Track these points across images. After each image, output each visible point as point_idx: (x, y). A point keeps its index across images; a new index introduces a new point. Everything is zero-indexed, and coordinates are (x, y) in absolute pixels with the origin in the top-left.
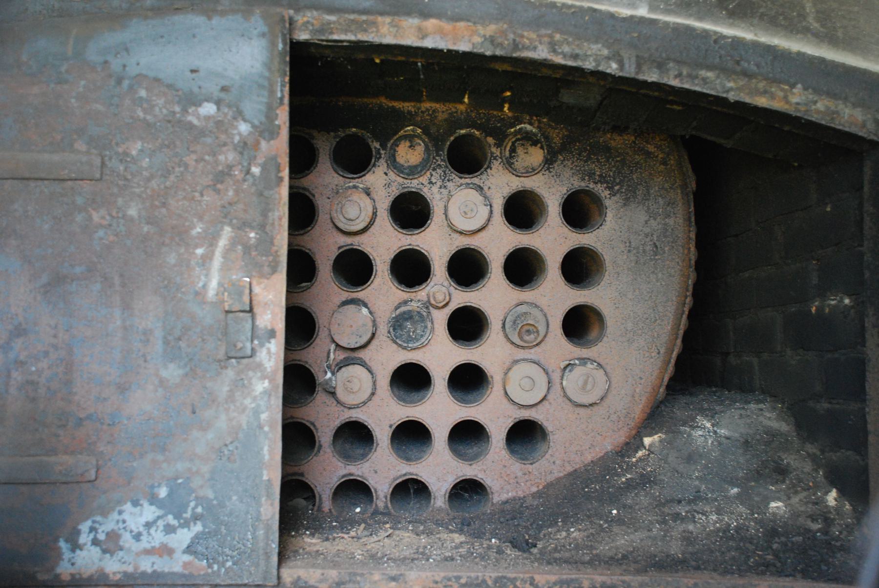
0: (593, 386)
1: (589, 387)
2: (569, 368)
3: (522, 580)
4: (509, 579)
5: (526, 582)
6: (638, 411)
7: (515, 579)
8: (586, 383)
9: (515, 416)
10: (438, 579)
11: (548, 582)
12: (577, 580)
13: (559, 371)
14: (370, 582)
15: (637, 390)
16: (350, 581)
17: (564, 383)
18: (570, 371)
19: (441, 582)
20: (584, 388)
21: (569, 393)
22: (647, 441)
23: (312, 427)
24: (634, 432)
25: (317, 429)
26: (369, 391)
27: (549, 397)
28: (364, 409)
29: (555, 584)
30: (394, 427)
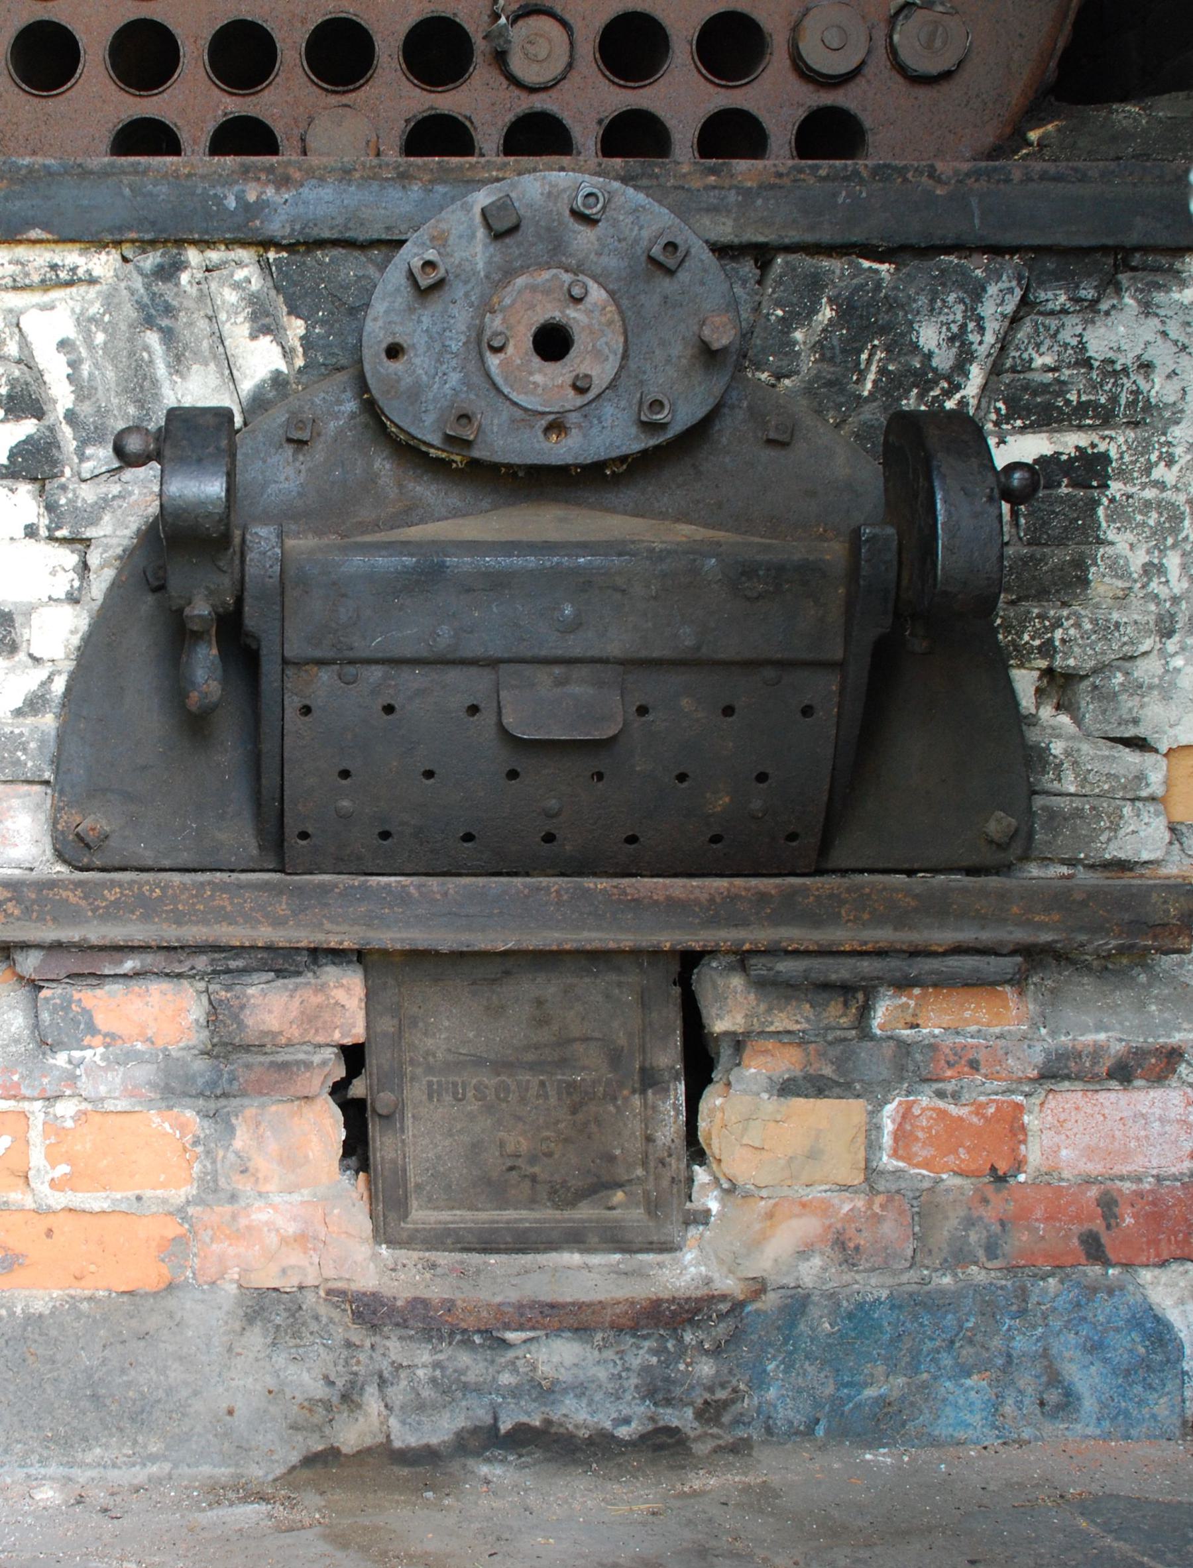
0: (945, 43)
1: (938, 43)
2: (905, 12)
3: (916, 170)
4: (895, 169)
5: (922, 174)
6: (1016, 94)
7: (905, 167)
8: (932, 37)
9: (809, 104)
10: (782, 170)
11: (956, 172)
12: (1003, 168)
13: (882, 25)
14: (675, 176)
15: (1015, 57)
16: (643, 175)
17: (896, 37)
18: (907, 17)
19: (788, 174)
20: (929, 45)
21: (906, 56)
22: (1033, 136)
23: (468, 124)
24: (1008, 130)
25: (475, 129)
26: (565, 60)
27: (866, 70)
28: (554, 93)
29: (968, 175)
30: (607, 122)
